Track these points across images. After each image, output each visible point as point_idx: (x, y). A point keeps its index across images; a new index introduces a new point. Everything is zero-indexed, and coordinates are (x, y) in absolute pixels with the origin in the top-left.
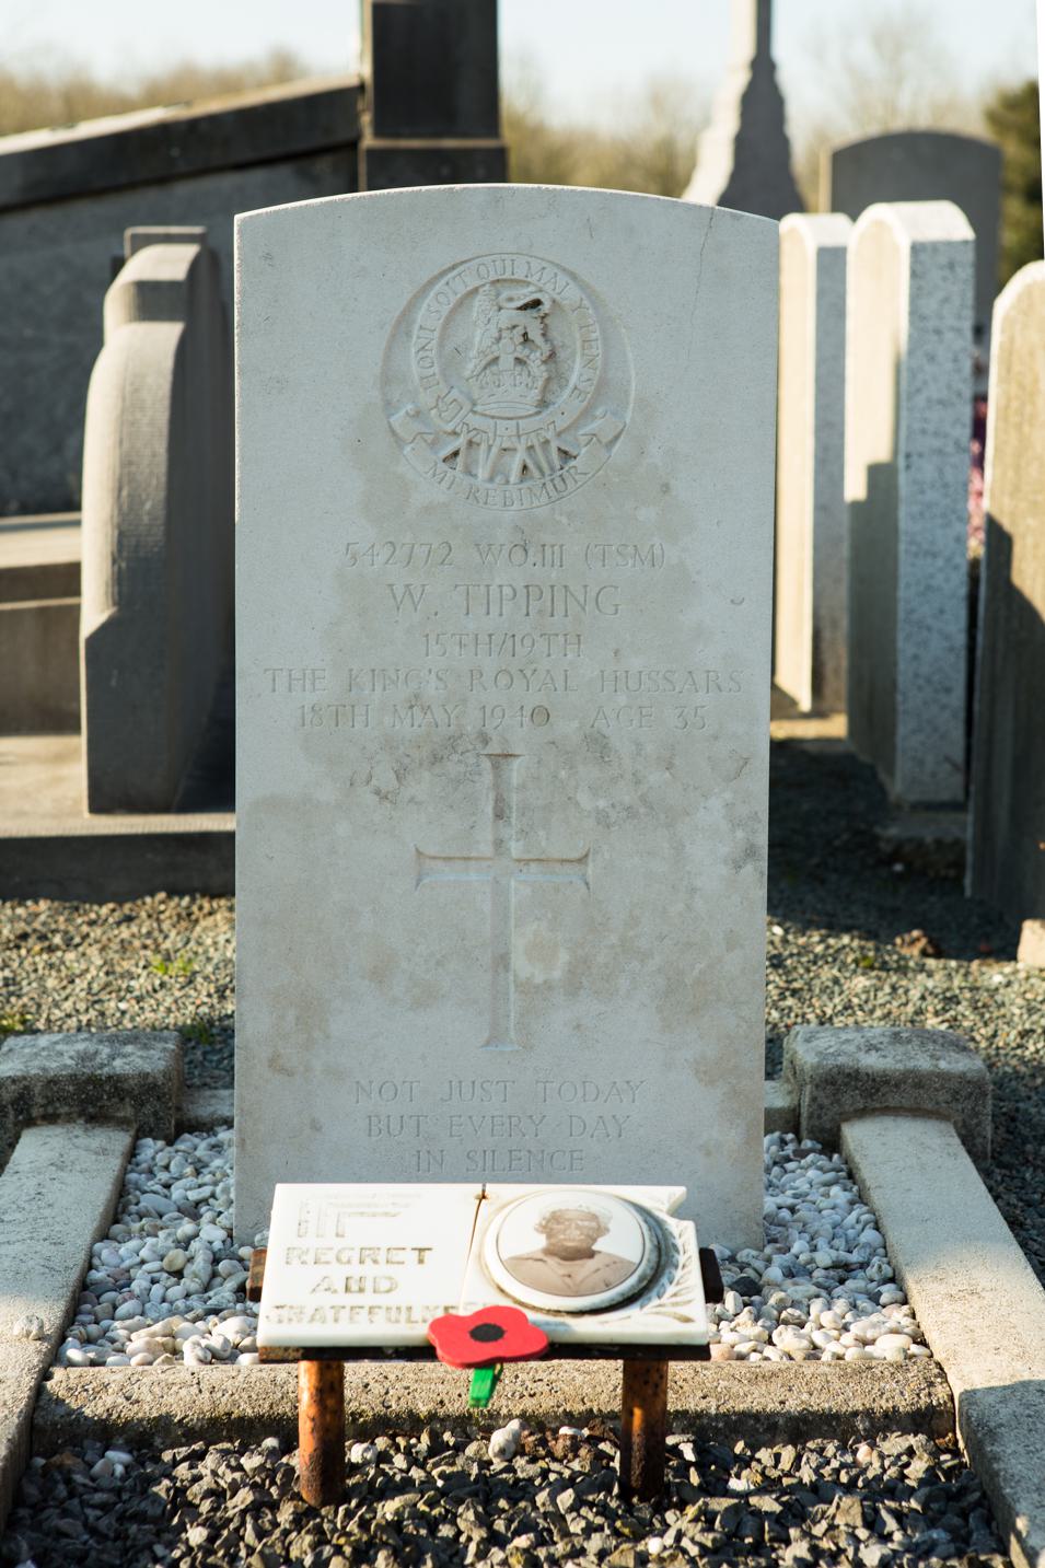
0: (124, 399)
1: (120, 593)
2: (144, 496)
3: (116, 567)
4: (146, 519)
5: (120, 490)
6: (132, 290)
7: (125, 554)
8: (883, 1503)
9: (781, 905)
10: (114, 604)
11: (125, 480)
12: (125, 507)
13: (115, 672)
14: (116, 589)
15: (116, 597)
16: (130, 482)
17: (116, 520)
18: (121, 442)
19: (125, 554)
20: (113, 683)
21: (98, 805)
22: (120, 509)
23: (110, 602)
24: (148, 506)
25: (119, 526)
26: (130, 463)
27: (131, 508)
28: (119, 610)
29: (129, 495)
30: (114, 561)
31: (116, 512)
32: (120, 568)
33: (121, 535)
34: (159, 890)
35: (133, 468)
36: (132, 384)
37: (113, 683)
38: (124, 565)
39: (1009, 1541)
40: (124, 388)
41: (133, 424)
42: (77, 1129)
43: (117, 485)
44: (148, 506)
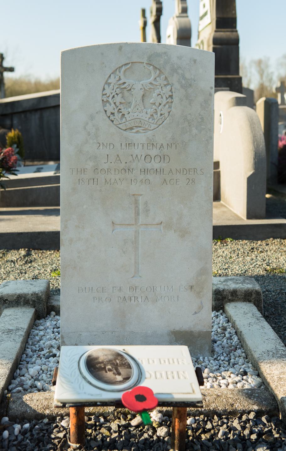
0: (250, 122)
1: (255, 167)
2: (260, 144)
3: (255, 161)
4: (261, 150)
5: (254, 143)
6: (235, 99)
7: (257, 158)
8: (84, 449)
9: (60, 306)
10: (254, 169)
11: (255, 140)
12: (256, 147)
13: (254, 186)
14: (255, 166)
15: (255, 168)
16: (256, 141)
17: (254, 150)
18: (252, 132)
19: (257, 158)
20: (253, 188)
21: (249, 217)
22: (255, 147)
23: (253, 169)
24: (261, 146)
25: (255, 151)
26: (255, 137)
27: (257, 147)
28: (255, 171)
29: (257, 144)
30: (254, 159)
31: (254, 148)
32: (255, 161)
33: (256, 153)
34: (271, 237)
35: (256, 138)
36: (250, 119)
37: (253, 188)
38: (256, 160)
39: (142, 440)
40: (249, 120)
41: (254, 127)
42: (248, 303)
43: (253, 141)
44: (261, 146)
